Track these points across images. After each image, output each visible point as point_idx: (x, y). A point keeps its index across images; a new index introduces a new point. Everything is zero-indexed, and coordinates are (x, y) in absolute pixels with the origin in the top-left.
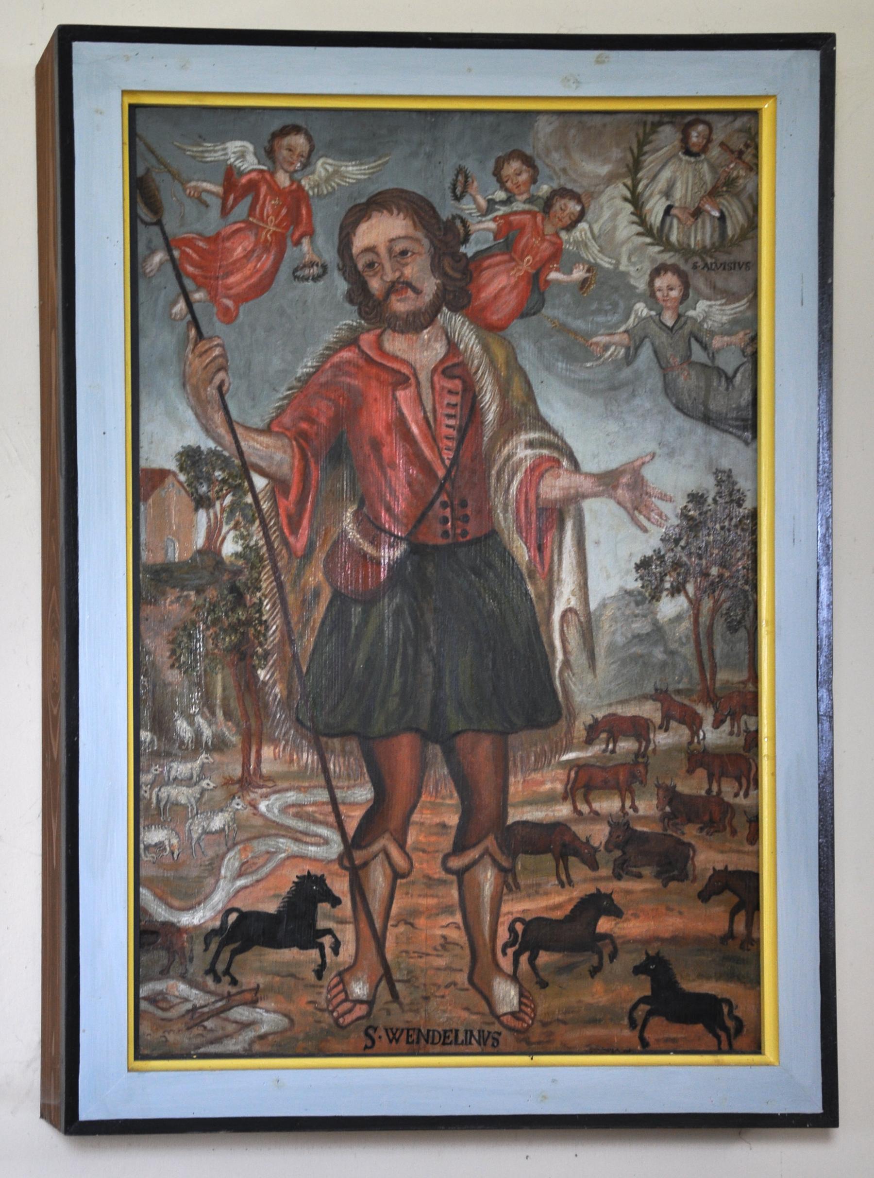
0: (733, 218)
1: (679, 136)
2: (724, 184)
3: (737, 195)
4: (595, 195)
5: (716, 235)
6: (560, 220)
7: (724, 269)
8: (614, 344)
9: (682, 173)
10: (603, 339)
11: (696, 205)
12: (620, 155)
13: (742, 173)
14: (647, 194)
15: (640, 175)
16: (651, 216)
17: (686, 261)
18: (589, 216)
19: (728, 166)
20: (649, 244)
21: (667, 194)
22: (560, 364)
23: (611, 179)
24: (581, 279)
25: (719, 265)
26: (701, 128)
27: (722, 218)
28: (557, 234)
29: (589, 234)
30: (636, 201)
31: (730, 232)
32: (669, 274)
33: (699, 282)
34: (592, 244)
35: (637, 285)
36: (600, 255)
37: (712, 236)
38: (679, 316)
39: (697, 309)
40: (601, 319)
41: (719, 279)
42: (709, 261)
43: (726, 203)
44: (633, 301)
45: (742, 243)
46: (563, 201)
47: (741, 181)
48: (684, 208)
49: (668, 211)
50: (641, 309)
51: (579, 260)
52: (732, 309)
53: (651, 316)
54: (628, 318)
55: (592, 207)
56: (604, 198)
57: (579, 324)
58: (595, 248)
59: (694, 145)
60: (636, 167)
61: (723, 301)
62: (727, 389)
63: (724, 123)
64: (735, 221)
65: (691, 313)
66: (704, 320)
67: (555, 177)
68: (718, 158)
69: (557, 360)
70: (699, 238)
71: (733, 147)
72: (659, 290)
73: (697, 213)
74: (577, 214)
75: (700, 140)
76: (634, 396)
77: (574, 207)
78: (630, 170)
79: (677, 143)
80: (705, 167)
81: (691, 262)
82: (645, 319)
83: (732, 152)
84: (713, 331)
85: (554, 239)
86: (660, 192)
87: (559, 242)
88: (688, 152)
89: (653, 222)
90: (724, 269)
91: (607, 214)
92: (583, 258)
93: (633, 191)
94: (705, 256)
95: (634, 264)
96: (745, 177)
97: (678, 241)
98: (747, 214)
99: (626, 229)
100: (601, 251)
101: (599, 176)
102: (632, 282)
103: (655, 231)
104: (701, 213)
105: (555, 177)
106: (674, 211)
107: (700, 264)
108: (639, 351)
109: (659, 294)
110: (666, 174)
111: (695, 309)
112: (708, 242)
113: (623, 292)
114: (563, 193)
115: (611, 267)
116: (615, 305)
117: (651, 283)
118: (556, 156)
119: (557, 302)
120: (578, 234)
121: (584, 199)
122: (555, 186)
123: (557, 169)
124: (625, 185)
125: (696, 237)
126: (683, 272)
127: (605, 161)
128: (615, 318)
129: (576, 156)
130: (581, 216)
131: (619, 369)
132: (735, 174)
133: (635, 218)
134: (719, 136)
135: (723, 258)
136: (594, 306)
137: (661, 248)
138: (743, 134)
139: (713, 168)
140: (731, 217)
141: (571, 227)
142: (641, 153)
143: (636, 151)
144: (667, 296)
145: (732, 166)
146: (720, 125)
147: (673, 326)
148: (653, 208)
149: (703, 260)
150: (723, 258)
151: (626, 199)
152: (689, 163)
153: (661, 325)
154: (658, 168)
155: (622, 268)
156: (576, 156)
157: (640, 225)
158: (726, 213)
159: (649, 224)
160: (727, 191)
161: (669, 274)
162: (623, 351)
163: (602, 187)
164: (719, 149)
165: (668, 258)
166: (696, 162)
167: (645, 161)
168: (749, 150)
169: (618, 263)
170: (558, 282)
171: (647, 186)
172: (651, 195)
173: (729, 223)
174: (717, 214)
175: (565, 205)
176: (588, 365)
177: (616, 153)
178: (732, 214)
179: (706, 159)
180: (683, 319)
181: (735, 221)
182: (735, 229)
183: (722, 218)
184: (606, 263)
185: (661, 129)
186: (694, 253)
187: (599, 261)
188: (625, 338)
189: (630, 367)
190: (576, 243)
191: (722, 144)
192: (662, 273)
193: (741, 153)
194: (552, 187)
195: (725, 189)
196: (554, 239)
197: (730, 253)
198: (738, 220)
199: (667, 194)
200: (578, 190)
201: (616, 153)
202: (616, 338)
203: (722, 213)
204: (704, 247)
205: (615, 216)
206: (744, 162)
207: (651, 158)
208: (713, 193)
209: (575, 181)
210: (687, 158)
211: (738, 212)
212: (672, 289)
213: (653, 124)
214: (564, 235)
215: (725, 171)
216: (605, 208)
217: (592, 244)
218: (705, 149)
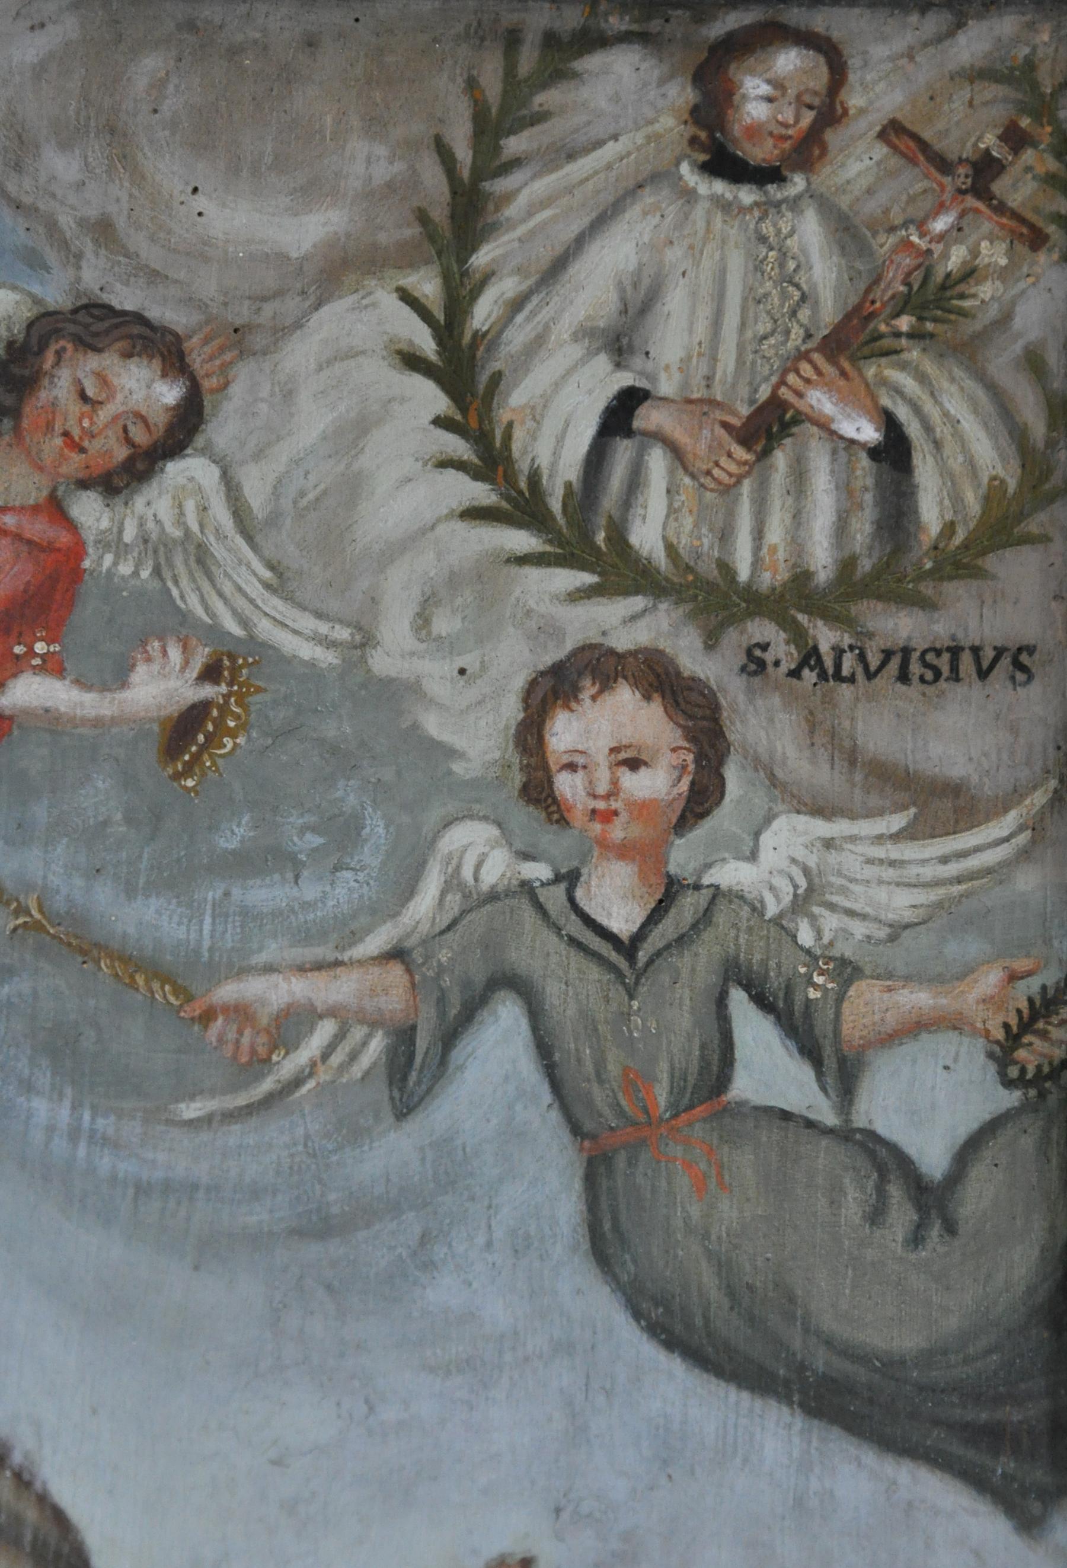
0: (950, 447)
1: (682, 94)
2: (903, 305)
3: (968, 353)
4: (259, 341)
5: (862, 528)
6: (72, 443)
7: (904, 677)
8: (332, 1012)
9: (694, 252)
10: (273, 992)
11: (764, 393)
12: (383, 172)
13: (994, 254)
14: (517, 337)
15: (482, 258)
16: (534, 436)
17: (711, 641)
18: (223, 429)
19: (921, 226)
20: (523, 560)
21: (619, 342)
22: (40, 1106)
23: (336, 272)
24: (173, 710)
25: (874, 661)
26: (788, 61)
27: (894, 451)
28: (55, 508)
29: (221, 513)
30: (461, 370)
31: (931, 511)
32: (625, 695)
33: (764, 726)
34: (231, 551)
35: (458, 742)
36: (275, 605)
37: (841, 529)
38: (670, 892)
39: (767, 856)
40: (265, 894)
41: (883, 723)
42: (826, 637)
43: (908, 382)
44: (434, 815)
45: (990, 562)
46: (93, 362)
47: (986, 290)
48: (699, 406)
49: (621, 415)
50: (481, 852)
51: (174, 624)
52: (944, 860)
53: (527, 888)
54: (409, 891)
55: (237, 390)
56: (300, 354)
57: (149, 920)
58: (243, 569)
59: (754, 132)
60: (465, 218)
61: (897, 822)
62: (916, 1239)
63: (899, 45)
64: (956, 463)
65: (731, 874)
66: (801, 904)
67: (52, 257)
68: (870, 191)
69: (28, 1087)
70: (775, 534)
71: (950, 146)
72: (572, 767)
73: (769, 426)
74: (160, 420)
75: (788, 115)
76: (429, 1266)
77: (146, 390)
78: (430, 233)
79: (669, 124)
80: (810, 232)
81: (734, 640)
82: (493, 896)
83: (943, 164)
84: (843, 962)
85: (39, 529)
86: (584, 333)
87: (64, 538)
88: (723, 164)
89: (544, 461)
90: (904, 677)
91: (313, 422)
92: (184, 617)
93: (448, 326)
94: (802, 618)
95: (447, 646)
96: (1004, 275)
97: (671, 549)
98: (1019, 436)
99: (410, 485)
100: (281, 581)
101: (283, 257)
102: (433, 725)
103: (556, 505)
104: (786, 428)
105: (52, 257)
106: (647, 418)
107: (782, 650)
108: (457, 1055)
109: (567, 785)
110: (615, 255)
111: (753, 856)
112: (822, 559)
113: (388, 774)
114: (96, 324)
115: (327, 658)
116: (344, 833)
117: (530, 735)
118: (61, 166)
119: (40, 812)
120: (164, 508)
121: (197, 361)
122: (55, 294)
123: (66, 221)
124: (407, 297)
125: (759, 534)
126: (695, 684)
127: (312, 192)
128: (344, 892)
129: (168, 171)
130: (184, 428)
131: (354, 1133)
132: (956, 258)
133: (457, 446)
134: (877, 92)
135: (900, 626)
136: (235, 835)
137: (588, 578)
138: (992, 91)
139: (847, 232)
140: (938, 445)
141: (127, 475)
142: (491, 162)
143: (464, 154)
144: (614, 792)
145: (940, 225)
146: (880, 51)
147: (639, 937)
148: (547, 400)
149: (797, 635)
150: (900, 626)
151: (412, 361)
152: (725, 206)
153: (574, 927)
154: (575, 228)
155: (381, 663)
156: (168, 171)
157: (477, 475)
158: (913, 429)
159: (523, 467)
160: (914, 335)
161: (625, 695)
162: (377, 1044)
163: (291, 305)
164: (881, 151)
165: (625, 623)
166: (768, 208)
167: (509, 197)
168: (1029, 156)
169: (366, 640)
170: (51, 722)
171: (517, 305)
172: (539, 341)
173: (926, 472)
174: (869, 433)
175: (103, 380)
176: (191, 1110)
177: (368, 161)
178: (942, 431)
179: (809, 193)
180: (688, 906)
181: (956, 463)
182: (957, 499)
183: (894, 451)
184: (297, 637)
185: (592, 62)
186: (756, 602)
187: (264, 629)
188: (392, 991)
189: (413, 1125)
190: (156, 548)
191: (893, 132)
192: (589, 688)
193: (986, 168)
194: (37, 301)
195: (904, 323)
196: (39, 529)
197: (927, 605)
198: (971, 464)
199: (619, 342)
200: (172, 316)
201: (368, 161)
202: (341, 989)
203: (890, 424)
204: (802, 577)
205: (353, 434)
206: (1001, 209)
207: (542, 186)
208: (850, 342)
209: (154, 276)
210: (719, 187)
211: (970, 426)
212: (634, 764)
213: (550, 40)
214: (89, 511)
215: (907, 244)
216: (304, 398)
217: (231, 551)
218: (807, 150)
